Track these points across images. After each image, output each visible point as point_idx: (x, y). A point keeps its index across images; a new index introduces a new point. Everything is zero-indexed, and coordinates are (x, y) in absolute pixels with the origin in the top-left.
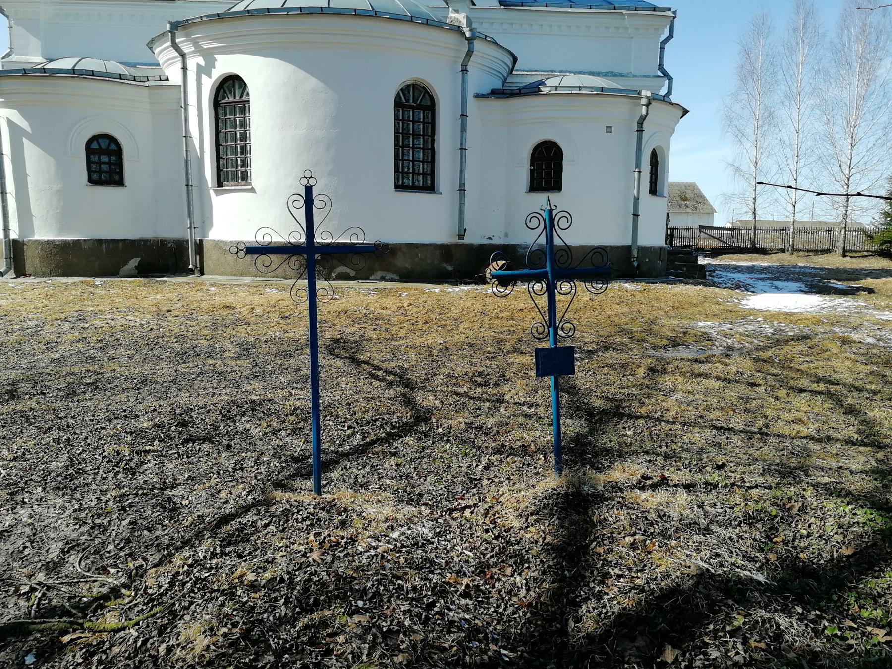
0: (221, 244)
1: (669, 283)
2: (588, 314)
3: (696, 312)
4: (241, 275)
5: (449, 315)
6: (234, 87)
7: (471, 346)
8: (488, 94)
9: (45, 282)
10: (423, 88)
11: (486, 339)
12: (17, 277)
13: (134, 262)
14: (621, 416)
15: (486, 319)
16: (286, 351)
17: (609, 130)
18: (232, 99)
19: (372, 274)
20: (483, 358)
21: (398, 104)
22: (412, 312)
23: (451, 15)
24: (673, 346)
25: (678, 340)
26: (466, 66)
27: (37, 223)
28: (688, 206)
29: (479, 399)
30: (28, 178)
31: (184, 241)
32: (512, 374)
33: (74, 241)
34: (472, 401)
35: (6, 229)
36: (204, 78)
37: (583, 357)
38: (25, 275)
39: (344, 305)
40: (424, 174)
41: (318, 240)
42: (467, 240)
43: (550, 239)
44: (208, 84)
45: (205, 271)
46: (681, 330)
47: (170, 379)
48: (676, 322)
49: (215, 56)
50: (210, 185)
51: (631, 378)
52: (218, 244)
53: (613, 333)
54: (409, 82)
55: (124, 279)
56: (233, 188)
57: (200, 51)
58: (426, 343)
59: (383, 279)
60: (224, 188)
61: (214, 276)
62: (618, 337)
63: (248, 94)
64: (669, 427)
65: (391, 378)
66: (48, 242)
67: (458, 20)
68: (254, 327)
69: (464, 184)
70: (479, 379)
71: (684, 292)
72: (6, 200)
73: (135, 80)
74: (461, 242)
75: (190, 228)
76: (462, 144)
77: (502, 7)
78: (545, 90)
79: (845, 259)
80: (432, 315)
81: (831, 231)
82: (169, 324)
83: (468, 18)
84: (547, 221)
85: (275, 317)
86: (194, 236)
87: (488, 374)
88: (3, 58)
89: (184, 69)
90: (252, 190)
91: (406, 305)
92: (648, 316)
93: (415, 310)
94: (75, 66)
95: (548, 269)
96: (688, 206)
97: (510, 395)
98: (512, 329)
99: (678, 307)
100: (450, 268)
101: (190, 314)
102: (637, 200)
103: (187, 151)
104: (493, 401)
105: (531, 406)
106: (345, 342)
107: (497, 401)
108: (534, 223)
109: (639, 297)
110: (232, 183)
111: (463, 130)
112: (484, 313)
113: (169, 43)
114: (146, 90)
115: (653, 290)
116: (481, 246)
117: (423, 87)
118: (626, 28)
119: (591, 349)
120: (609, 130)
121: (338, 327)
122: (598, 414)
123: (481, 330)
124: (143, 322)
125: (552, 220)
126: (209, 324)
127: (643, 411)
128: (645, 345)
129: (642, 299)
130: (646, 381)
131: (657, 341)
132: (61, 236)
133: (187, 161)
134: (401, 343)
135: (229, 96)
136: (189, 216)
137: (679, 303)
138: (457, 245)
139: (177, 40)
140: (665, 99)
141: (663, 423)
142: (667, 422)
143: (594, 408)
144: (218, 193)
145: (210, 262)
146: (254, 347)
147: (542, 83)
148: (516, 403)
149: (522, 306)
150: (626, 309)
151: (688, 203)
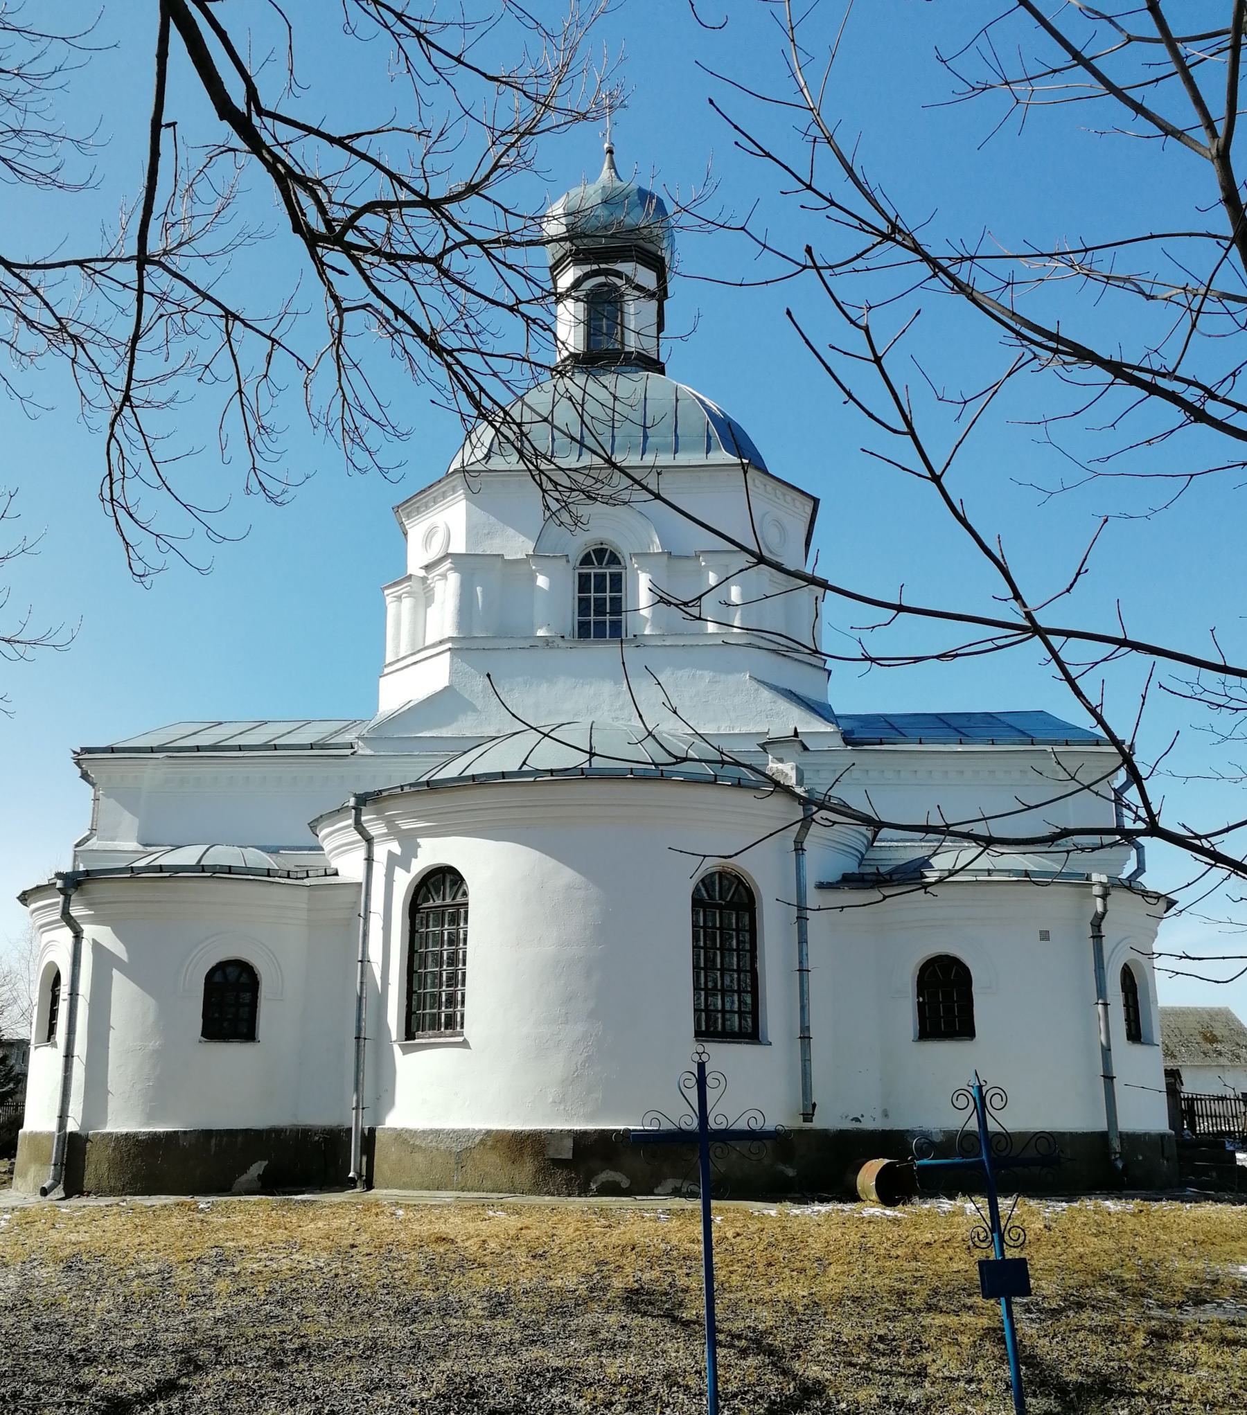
0: (406, 1136)
1: (1184, 1200)
2: (1044, 1251)
3: (1237, 1250)
5: (805, 1253)
6: (444, 884)
7: (855, 1300)
8: (838, 882)
9: (118, 1205)
10: (736, 877)
11: (877, 1289)
12: (68, 1196)
13: (257, 1169)
14: (1109, 1393)
15: (871, 1260)
16: (561, 1307)
18: (439, 902)
19: (658, 1184)
20: (879, 1317)
21: (697, 902)
22: (742, 1246)
23: (771, 765)
24: (1195, 1304)
25: (1203, 1293)
26: (802, 843)
27: (113, 1104)
28: (1220, 1054)
29: (887, 1372)
31: (340, 1131)
32: (932, 1340)
33: (168, 1134)
34: (877, 1375)
35: (63, 1117)
36: (399, 872)
37: (1042, 1317)
38: (81, 1193)
39: (628, 1236)
40: (740, 1013)
41: (712, 1125)
42: (818, 1123)
43: (982, 1122)
44: (404, 881)
45: (375, 1183)
46: (1208, 1277)
47: (409, 1344)
48: (1200, 1265)
49: (419, 840)
50: (394, 1036)
51: (1125, 1347)
52: (403, 1137)
53: (1090, 1283)
54: (714, 870)
55: (243, 1198)
56: (433, 1040)
57: (394, 832)
58: (780, 1295)
59: (676, 1193)
60: (417, 1041)
62: (1099, 1288)
63: (465, 894)
64: (1182, 1406)
65: (743, 1343)
66: (127, 1136)
67: (782, 772)
68: (495, 1272)
69: (808, 1028)
70: (881, 1346)
71: (1214, 1216)
72: (71, 1067)
73: (288, 877)
74: (808, 1125)
75: (357, 1108)
76: (801, 962)
77: (849, 748)
78: (932, 876)
80: (776, 1253)
82: (362, 1266)
83: (797, 768)
84: (977, 1099)
85: (522, 1257)
86: (350, 1120)
87: (894, 1340)
88: (77, 846)
89: (369, 860)
90: (465, 1044)
91: (730, 1235)
92: (1149, 1256)
93: (746, 1244)
94: (200, 860)
95: (984, 1157)
96: (1220, 1054)
97: (935, 1367)
98: (919, 1274)
99: (1203, 1242)
100: (791, 1172)
101: (386, 1251)
102: (1106, 1050)
103: (362, 983)
104: (910, 1375)
105: (970, 1381)
106: (647, 1293)
107: (918, 1374)
108: (962, 1102)
109: (1131, 1223)
110: (430, 1032)
111: (803, 940)
112: (865, 1250)
113: (351, 822)
114: (305, 893)
115: (1156, 1211)
116: (842, 1133)
117: (736, 876)
119: (1054, 1306)
120: (1045, 936)
121: (628, 1270)
122: (1074, 1390)
123: (866, 1275)
124: (322, 1265)
125: (983, 1099)
126: (423, 1267)
127: (1143, 1386)
128: (1146, 1301)
129: (1138, 1227)
130: (1149, 1352)
131: (1165, 1297)
132: (147, 1124)
133: (360, 999)
134: (739, 1295)
135: (435, 897)
136: (357, 1090)
137: (1206, 1233)
138: (800, 1132)
139: (363, 818)
140: (1130, 886)
141: (1173, 1402)
142: (1182, 1401)
143: (1067, 1384)
144: (406, 1050)
145: (386, 1166)
146: (509, 1301)
147: (925, 863)
148: (945, 1378)
149: (928, 1237)
150: (1109, 1244)
151: (1219, 1047)
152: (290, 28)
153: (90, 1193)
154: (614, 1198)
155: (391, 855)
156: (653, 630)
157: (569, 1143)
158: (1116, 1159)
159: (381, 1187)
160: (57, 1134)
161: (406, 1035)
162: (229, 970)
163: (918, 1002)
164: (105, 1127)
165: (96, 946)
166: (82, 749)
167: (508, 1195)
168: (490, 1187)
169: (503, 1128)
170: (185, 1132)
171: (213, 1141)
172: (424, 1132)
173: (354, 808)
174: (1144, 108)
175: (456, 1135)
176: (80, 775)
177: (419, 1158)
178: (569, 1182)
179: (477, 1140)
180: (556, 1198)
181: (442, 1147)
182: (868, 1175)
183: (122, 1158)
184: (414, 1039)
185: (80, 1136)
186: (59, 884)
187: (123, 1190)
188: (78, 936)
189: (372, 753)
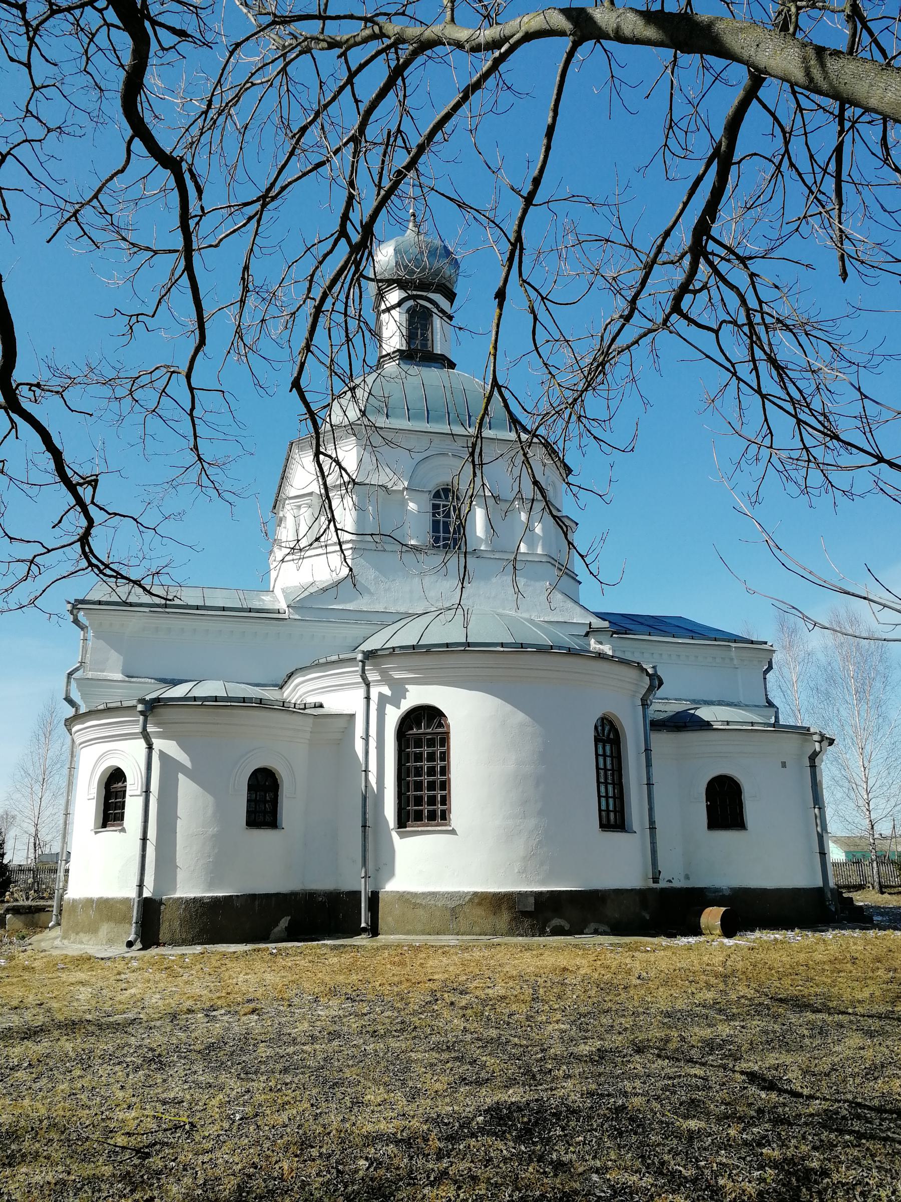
4: (438, 934)
13: (284, 923)
17: (784, 765)
30: (179, 820)
33: (225, 897)
35: (141, 886)
44: (393, 716)
45: (380, 931)
49: (407, 686)
52: (405, 898)
57: (386, 679)
59: (596, 932)
60: (408, 829)
61: (397, 937)
66: (195, 900)
74: (655, 886)
79: (884, 896)
81: (858, 863)
86: (363, 888)
89: (368, 698)
90: (453, 832)
114: (310, 720)
118: (732, 659)
120: (784, 765)
132: (209, 891)
144: (402, 836)
152: (47, 60)
153: (165, 944)
154: (563, 937)
155: (381, 696)
156: (486, 547)
157: (532, 900)
158: (830, 905)
159: (387, 934)
160: (137, 900)
161: (398, 824)
162: (259, 777)
163: (707, 805)
164: (175, 893)
165: (162, 755)
166: (76, 600)
167: (491, 937)
168: (479, 932)
169: (483, 890)
170: (237, 896)
171: (257, 903)
172: (423, 894)
173: (361, 661)
174: (181, 223)
175: (451, 896)
176: (72, 620)
177: (420, 912)
178: (532, 927)
179: (467, 899)
180: (524, 938)
181: (440, 904)
182: (712, 916)
183: (191, 916)
184: (406, 827)
185: (155, 900)
186: (140, 707)
187: (193, 941)
188: (150, 747)
189: (299, 618)
